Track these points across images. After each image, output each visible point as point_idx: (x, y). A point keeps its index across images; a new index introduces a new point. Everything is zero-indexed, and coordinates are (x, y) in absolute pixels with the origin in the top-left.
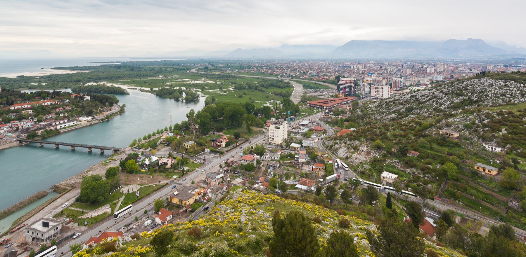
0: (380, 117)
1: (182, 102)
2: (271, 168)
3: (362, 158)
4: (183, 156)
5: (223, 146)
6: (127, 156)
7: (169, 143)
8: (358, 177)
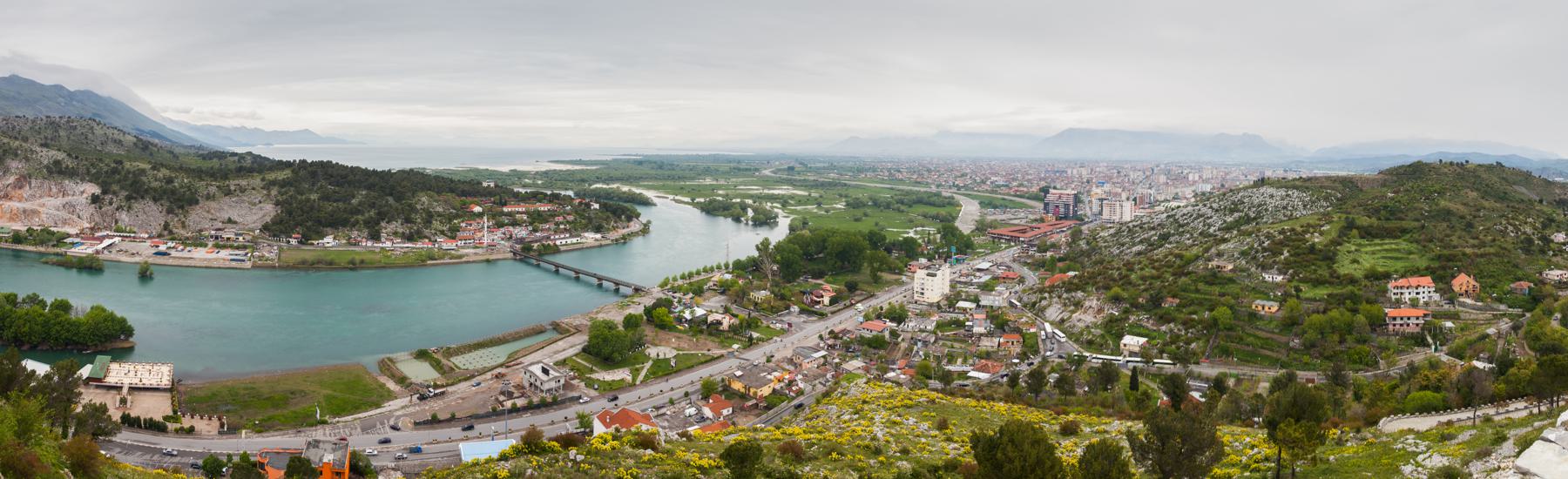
0: (1118, 251)
1: (747, 224)
2: (920, 344)
3: (1089, 318)
4: (749, 314)
5: (825, 303)
6: (655, 301)
7: (724, 290)
8: (1082, 350)
